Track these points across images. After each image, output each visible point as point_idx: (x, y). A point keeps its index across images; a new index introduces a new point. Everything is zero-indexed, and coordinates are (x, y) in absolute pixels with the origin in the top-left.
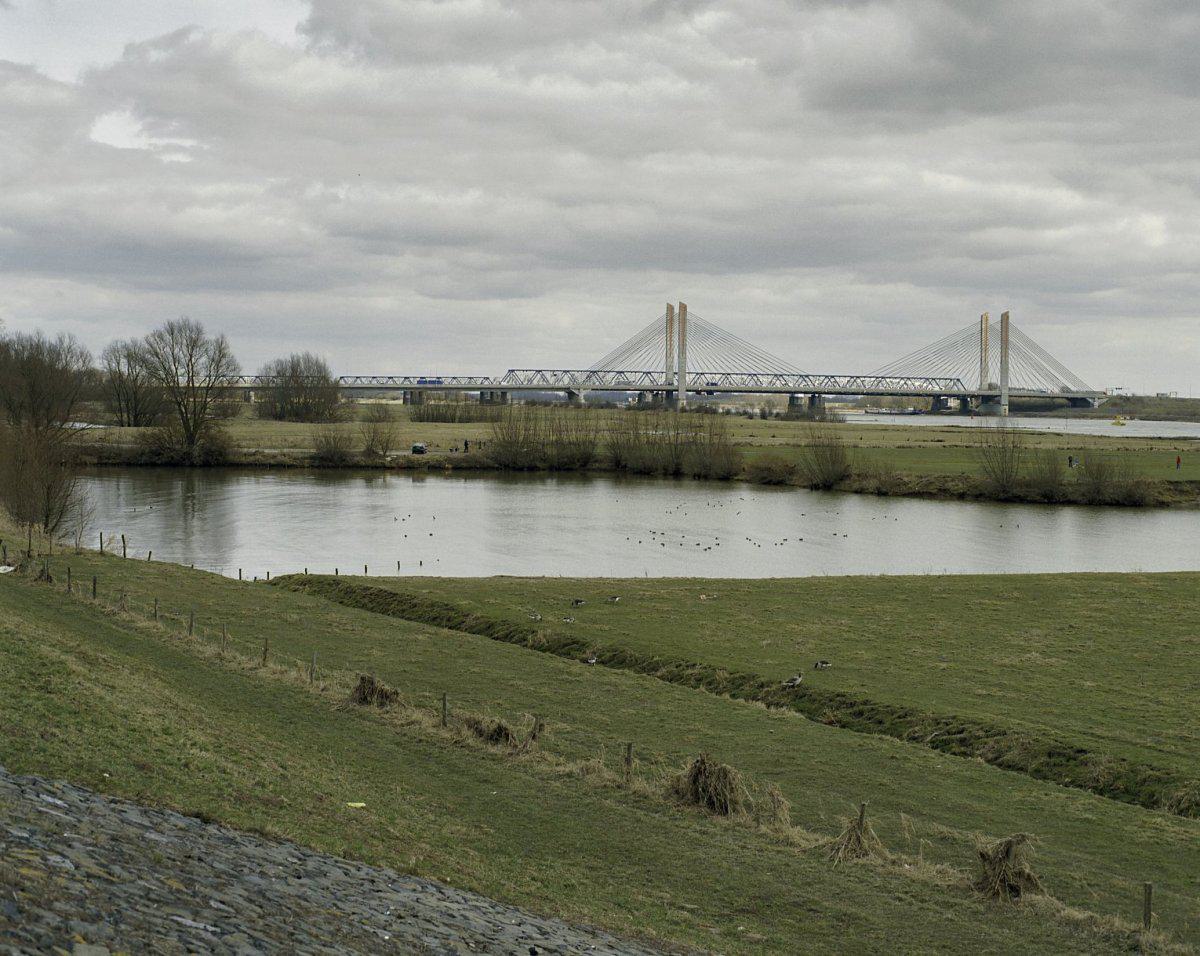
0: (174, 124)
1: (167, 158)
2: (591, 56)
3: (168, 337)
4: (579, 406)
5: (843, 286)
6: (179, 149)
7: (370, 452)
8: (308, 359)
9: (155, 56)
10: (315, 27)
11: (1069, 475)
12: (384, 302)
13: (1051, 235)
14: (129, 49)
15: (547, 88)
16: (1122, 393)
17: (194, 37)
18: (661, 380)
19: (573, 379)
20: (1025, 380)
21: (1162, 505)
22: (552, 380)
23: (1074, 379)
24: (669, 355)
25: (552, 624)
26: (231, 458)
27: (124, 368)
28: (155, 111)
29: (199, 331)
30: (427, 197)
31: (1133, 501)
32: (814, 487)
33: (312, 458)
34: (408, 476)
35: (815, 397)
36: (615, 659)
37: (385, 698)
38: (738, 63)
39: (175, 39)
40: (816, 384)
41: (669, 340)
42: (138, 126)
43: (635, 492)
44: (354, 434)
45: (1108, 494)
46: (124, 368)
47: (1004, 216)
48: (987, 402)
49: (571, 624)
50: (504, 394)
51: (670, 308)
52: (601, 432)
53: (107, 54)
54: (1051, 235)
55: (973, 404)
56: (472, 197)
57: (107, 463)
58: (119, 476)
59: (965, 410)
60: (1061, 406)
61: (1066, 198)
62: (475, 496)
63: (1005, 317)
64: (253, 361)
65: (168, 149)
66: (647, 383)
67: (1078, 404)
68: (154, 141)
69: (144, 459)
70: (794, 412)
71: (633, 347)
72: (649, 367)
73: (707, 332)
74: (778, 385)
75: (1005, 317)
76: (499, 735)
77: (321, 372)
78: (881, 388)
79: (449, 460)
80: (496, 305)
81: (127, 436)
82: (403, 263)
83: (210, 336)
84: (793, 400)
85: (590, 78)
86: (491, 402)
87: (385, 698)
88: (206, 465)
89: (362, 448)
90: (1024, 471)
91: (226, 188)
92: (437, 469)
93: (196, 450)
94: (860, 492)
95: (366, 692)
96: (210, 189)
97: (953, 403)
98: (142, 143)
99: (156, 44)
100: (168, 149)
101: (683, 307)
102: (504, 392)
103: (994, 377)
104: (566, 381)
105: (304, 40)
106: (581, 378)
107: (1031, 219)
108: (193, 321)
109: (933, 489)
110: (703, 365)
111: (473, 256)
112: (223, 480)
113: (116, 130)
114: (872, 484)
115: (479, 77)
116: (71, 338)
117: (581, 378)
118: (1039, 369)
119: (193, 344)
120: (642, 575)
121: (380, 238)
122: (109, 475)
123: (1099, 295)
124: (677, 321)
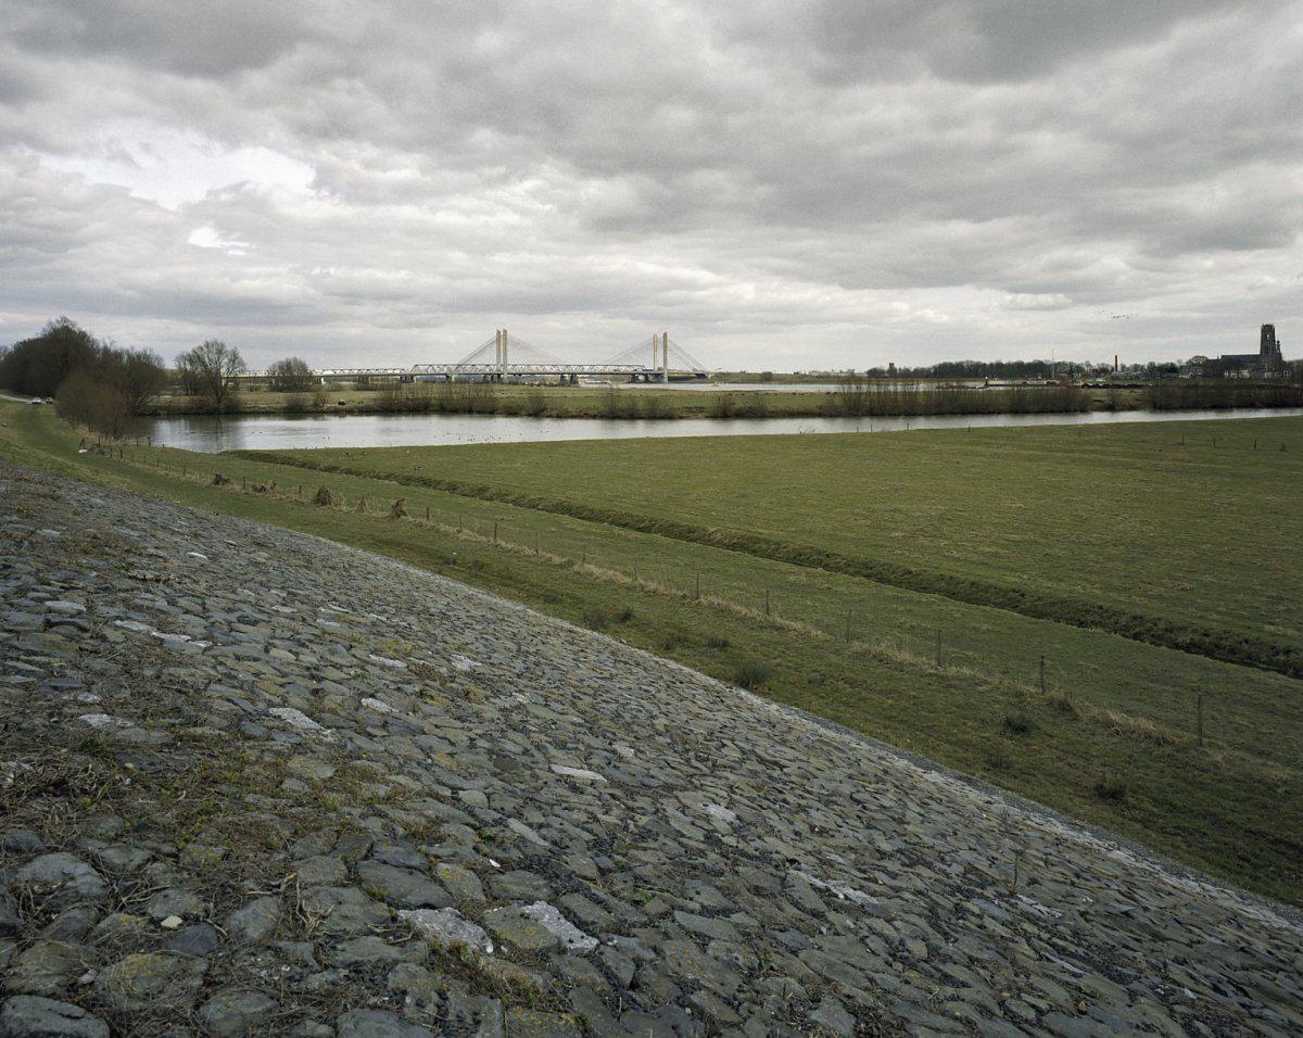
0: (238, 234)
1: (231, 253)
2: (467, 202)
3: (205, 349)
4: (450, 383)
5: (595, 320)
6: (238, 248)
7: (315, 405)
8: (295, 360)
9: (224, 197)
10: (318, 184)
11: (641, 405)
12: (354, 330)
13: (700, 294)
14: (210, 193)
15: (445, 218)
16: (722, 371)
17: (247, 187)
18: (495, 369)
19: (449, 369)
20: (676, 365)
21: (681, 418)
22: (438, 370)
23: (698, 364)
24: (498, 356)
25: (345, 464)
26: (240, 409)
27: (188, 367)
28: (225, 227)
29: (223, 346)
30: (379, 274)
31: (669, 416)
32: (530, 415)
33: (285, 408)
34: (335, 415)
35: (573, 375)
36: (349, 472)
37: (226, 481)
38: (547, 207)
39: (236, 188)
40: (574, 369)
41: (499, 348)
42: (217, 235)
43: (49, 329)
44: (308, 398)
45: (658, 413)
46: (188, 367)
47: (679, 284)
48: (658, 377)
49: (331, 461)
50: (412, 378)
51: (499, 332)
52: (435, 393)
53: (197, 194)
54: (700, 294)
55: (651, 378)
56: (403, 274)
57: (173, 413)
58: (180, 419)
59: (647, 381)
60: (692, 378)
61: (706, 276)
62: (372, 422)
63: (665, 335)
64: (259, 364)
65: (232, 247)
66: (487, 370)
67: (701, 377)
68: (224, 243)
69: (194, 411)
70: (562, 382)
71: (482, 351)
72: (488, 362)
73: (516, 344)
74: (554, 370)
75: (665, 335)
76: (263, 489)
77: (303, 367)
78: (606, 371)
79: (357, 408)
80: (415, 331)
81: (184, 400)
82: (365, 309)
83: (229, 348)
84: (563, 377)
85: (467, 213)
86: (406, 381)
87: (226, 481)
88: (227, 413)
89: (311, 402)
90: (622, 405)
91: (264, 269)
92: (350, 412)
93: (222, 406)
94: (550, 416)
95: (218, 480)
96: (255, 270)
97: (641, 378)
98: (218, 244)
99: (225, 190)
100: (232, 247)
101: (505, 331)
102: (412, 376)
103: (662, 366)
104: (445, 370)
105: (312, 193)
106: (453, 368)
107: (692, 285)
108: (219, 341)
109: (582, 414)
110: (517, 361)
111: (403, 306)
112: (237, 419)
113: (204, 237)
114: (554, 413)
115: (408, 212)
116: (109, 338)
117: (453, 368)
118: (680, 358)
119: (220, 352)
120: (389, 446)
121: (353, 296)
122: (175, 420)
123: (720, 324)
124: (501, 339)
